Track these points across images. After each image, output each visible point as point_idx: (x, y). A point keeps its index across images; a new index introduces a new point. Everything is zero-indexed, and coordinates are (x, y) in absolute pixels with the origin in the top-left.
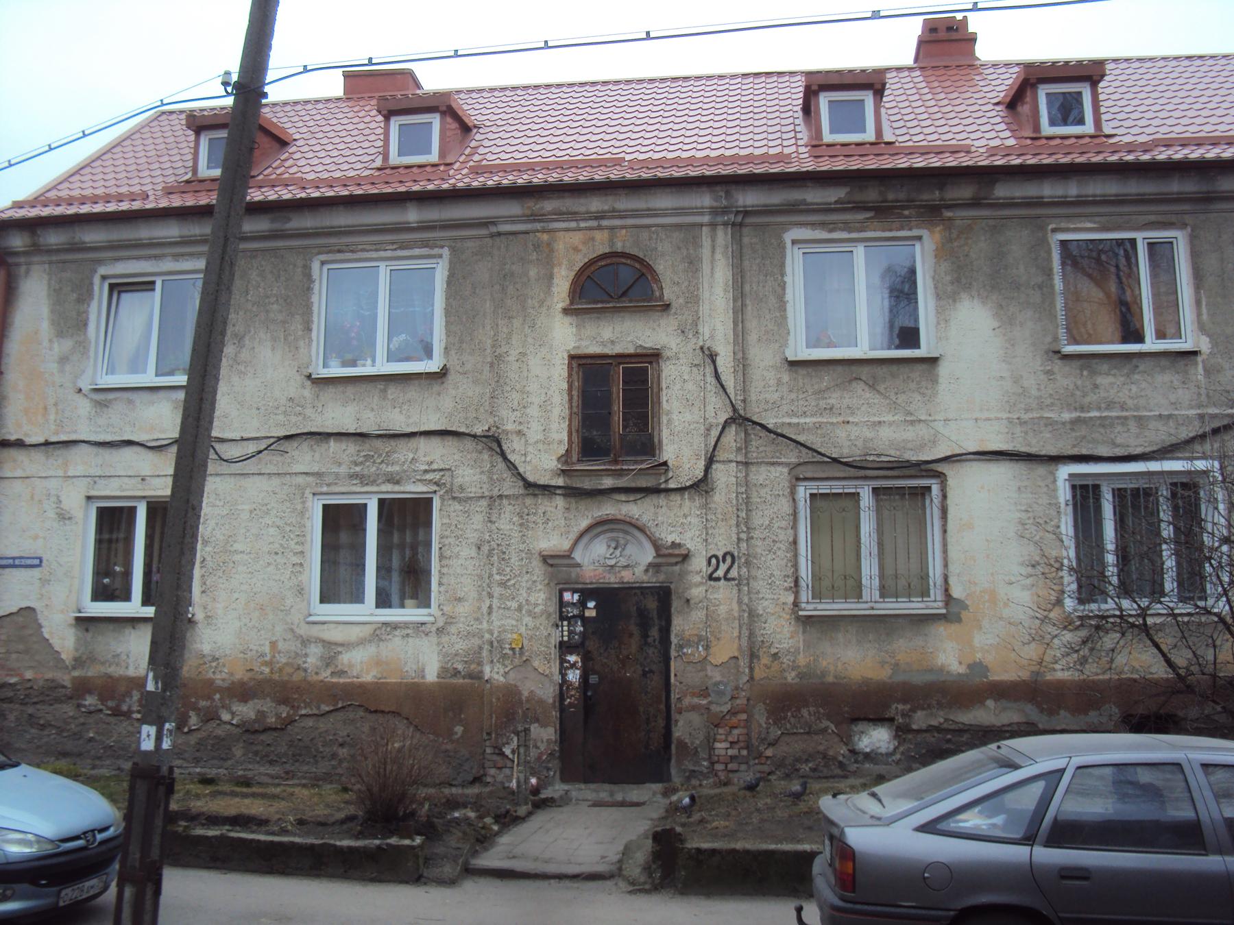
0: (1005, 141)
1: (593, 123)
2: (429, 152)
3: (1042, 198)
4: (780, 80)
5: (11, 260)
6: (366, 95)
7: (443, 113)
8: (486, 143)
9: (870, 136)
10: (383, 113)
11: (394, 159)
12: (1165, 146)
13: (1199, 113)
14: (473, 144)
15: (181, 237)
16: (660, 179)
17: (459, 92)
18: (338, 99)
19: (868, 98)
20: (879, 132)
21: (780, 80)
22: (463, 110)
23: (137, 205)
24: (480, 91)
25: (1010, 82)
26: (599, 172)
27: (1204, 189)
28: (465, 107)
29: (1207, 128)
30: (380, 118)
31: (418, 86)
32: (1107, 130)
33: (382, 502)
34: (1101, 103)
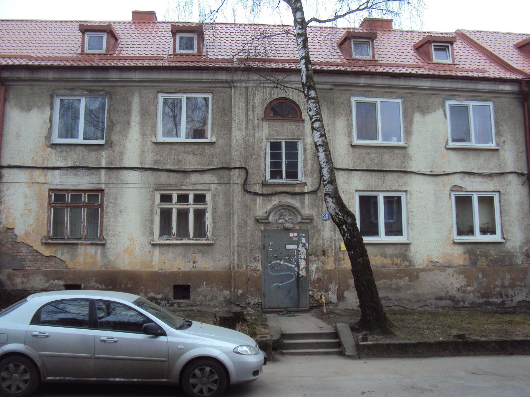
0: (336, 60)
1: (133, 40)
2: (436, 59)
3: (109, 79)
4: (231, 27)
5: (7, 83)
6: (147, 21)
7: (108, 33)
8: (124, 49)
9: (369, 57)
10: (174, 31)
11: (87, 51)
12: (324, 65)
13: (392, 53)
14: (119, 49)
15: (53, 78)
16: (177, 67)
17: (115, 22)
18: (129, 22)
19: (449, 45)
20: (374, 57)
21: (231, 27)
22: (116, 33)
23: (481, 75)
24: (66, 22)
25: (342, 35)
26: (146, 62)
27: (31, 76)
28: (117, 32)
29: (390, 59)
30: (81, 34)
31: (156, 20)
32: (456, 62)
33: (286, 143)
34: (455, 51)
